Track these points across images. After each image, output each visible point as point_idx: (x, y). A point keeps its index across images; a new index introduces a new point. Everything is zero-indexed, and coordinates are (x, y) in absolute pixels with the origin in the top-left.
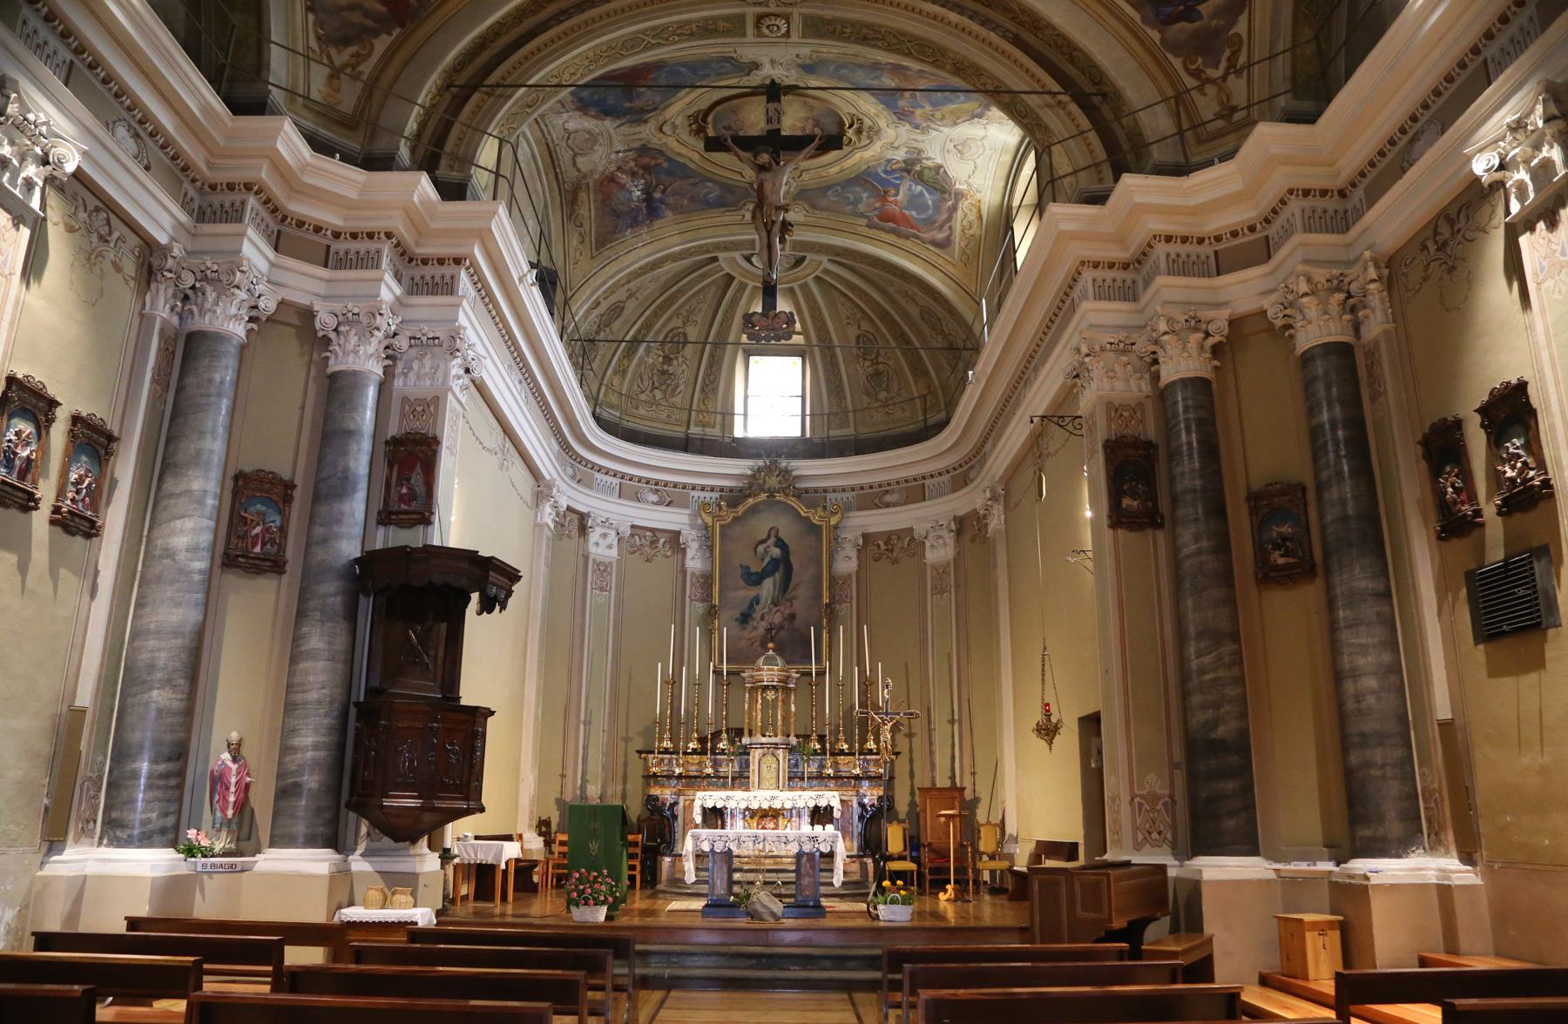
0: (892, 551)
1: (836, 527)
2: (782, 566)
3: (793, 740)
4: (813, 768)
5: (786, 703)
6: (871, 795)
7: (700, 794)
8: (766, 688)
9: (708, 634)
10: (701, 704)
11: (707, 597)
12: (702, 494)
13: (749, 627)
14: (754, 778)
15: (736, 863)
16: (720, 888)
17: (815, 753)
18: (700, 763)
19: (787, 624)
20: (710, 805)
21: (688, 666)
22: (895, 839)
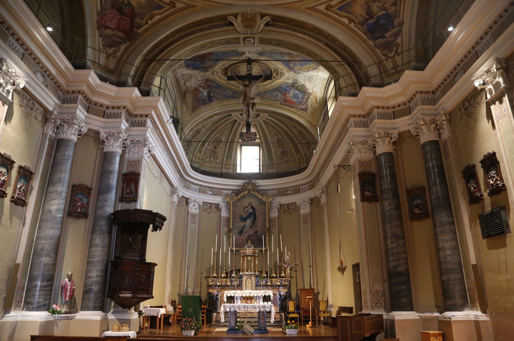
0: (289, 210)
1: (271, 202)
2: (253, 215)
4: (264, 283)
5: (254, 261)
7: (226, 292)
8: (248, 255)
9: (228, 238)
11: (228, 226)
12: (227, 191)
13: (242, 235)
14: (244, 286)
15: (238, 315)
16: (233, 324)
17: (264, 277)
18: (226, 281)
19: (255, 235)
20: (229, 295)
21: (223, 249)
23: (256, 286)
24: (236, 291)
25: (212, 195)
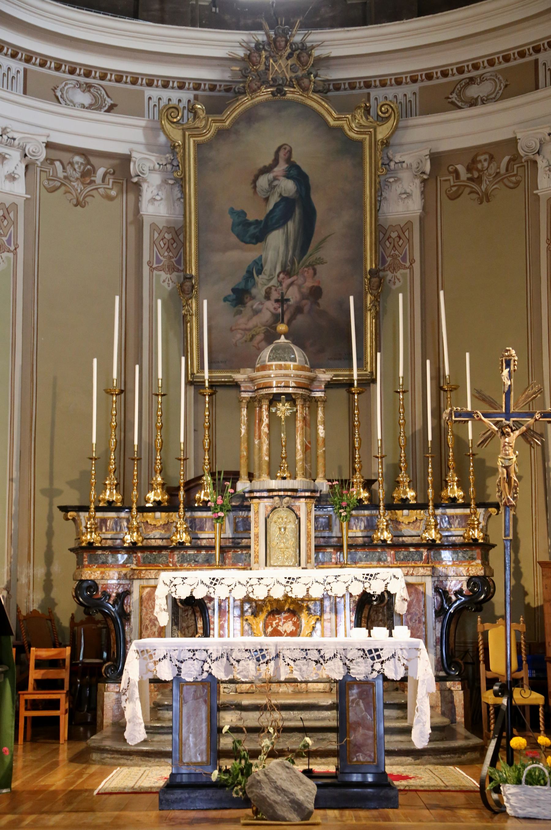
0: (478, 180)
1: (386, 144)
2: (299, 209)
3: (323, 485)
4: (357, 532)
5: (310, 423)
6: (457, 574)
7: (165, 576)
8: (275, 399)
9: (180, 323)
10: (168, 425)
11: (178, 264)
12: (166, 94)
13: (247, 311)
14: (258, 547)
15: (227, 694)
16: (195, 749)
17: (360, 505)
18: (167, 526)
19: (307, 305)
20: (183, 593)
21: (142, 365)
22: (500, 648)
23: (318, 548)
24: (218, 573)
25: (90, 107)
